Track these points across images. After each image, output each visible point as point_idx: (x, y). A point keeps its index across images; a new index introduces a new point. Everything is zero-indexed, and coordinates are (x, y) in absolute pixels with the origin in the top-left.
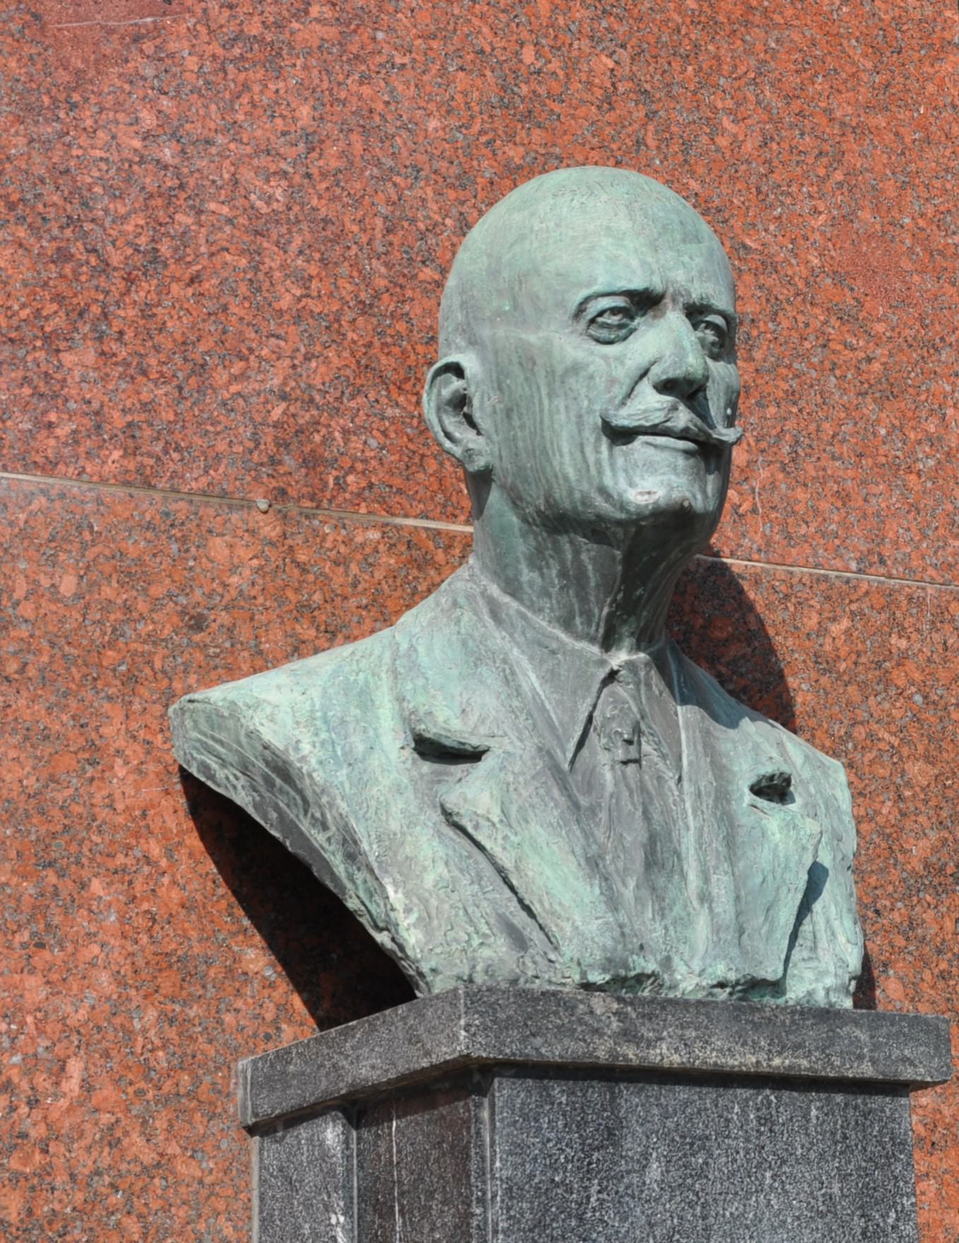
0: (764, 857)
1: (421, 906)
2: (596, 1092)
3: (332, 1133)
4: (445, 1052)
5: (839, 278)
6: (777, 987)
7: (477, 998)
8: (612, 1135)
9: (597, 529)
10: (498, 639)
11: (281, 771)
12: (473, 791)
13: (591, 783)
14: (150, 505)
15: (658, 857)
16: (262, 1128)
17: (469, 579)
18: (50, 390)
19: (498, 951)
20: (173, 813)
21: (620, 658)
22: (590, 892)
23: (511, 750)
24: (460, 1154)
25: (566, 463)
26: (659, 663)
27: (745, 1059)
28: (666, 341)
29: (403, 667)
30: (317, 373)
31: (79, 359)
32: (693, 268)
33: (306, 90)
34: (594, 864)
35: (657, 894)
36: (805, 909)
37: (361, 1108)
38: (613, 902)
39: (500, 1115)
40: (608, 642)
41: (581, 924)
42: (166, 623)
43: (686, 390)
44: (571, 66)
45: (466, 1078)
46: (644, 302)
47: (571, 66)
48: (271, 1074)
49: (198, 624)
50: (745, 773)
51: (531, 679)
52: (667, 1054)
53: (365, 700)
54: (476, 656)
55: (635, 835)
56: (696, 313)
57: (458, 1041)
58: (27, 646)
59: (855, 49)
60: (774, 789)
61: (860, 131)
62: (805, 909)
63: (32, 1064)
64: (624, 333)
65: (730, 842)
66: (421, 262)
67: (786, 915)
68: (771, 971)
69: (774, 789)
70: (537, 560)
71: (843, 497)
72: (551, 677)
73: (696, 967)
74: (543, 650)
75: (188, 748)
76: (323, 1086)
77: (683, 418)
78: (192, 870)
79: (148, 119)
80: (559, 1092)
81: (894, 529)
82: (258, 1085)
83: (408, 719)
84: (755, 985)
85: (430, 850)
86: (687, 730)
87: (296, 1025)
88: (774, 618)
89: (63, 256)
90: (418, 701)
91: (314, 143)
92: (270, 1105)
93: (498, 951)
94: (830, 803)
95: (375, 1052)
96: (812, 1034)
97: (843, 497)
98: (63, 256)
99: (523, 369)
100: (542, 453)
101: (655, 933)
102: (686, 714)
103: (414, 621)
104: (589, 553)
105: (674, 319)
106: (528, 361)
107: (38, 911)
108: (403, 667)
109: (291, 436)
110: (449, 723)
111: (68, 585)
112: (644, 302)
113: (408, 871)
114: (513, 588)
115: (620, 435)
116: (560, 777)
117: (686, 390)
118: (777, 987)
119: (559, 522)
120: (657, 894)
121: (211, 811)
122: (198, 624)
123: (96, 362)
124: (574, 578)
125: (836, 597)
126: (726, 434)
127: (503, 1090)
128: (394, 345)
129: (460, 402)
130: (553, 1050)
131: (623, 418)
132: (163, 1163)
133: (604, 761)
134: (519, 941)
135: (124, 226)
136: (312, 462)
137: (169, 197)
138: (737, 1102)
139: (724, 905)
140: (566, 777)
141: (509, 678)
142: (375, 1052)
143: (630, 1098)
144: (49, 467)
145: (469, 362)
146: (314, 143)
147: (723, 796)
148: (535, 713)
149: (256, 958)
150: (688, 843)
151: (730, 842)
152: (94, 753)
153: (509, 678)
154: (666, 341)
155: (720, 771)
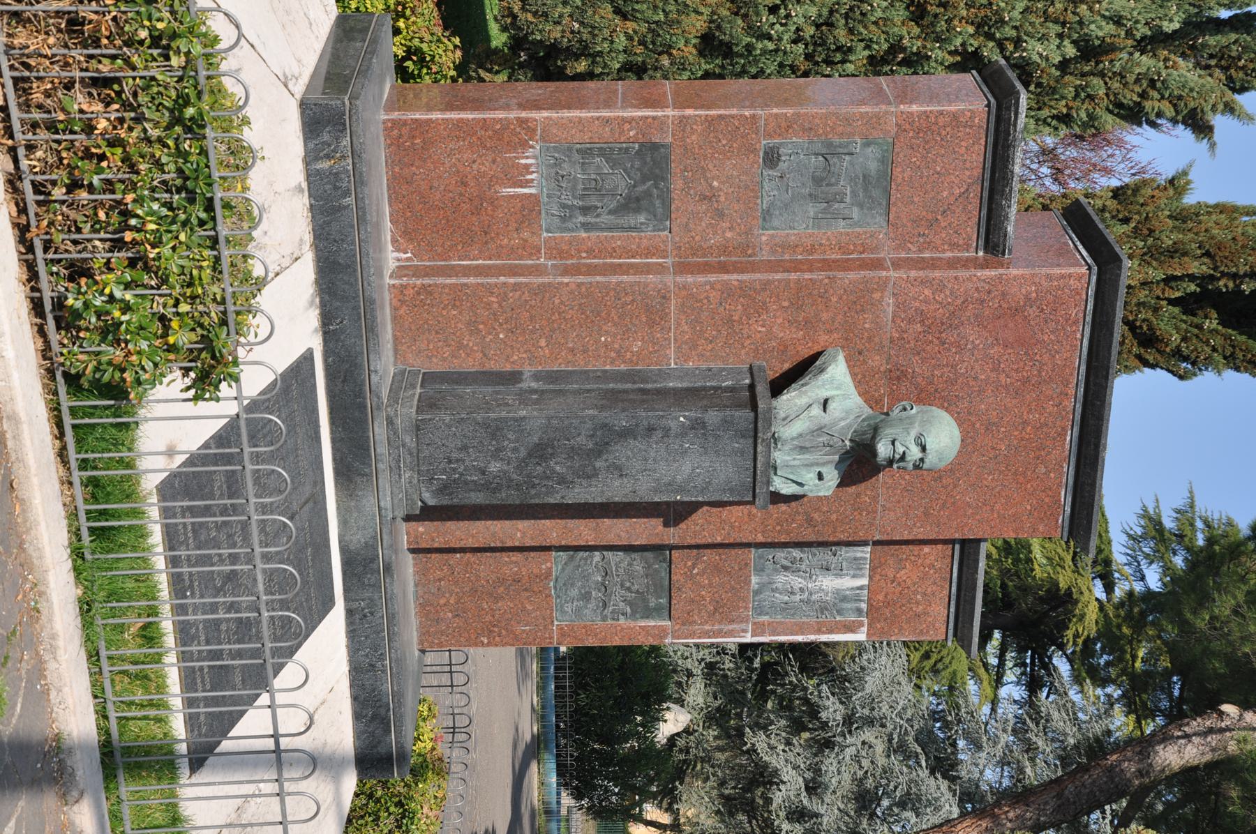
0: (804, 473)
1: (791, 399)
2: (752, 433)
3: (747, 381)
4: (759, 403)
5: (953, 503)
6: (775, 474)
7: (770, 410)
8: (743, 437)
9: (874, 438)
10: (852, 417)
11: (822, 370)
12: (816, 411)
13: (819, 435)
14: (886, 343)
15: (803, 449)
16: (751, 368)
17: (868, 411)
18: (911, 321)
19: (782, 415)
20: (817, 349)
21: (848, 443)
22: (795, 434)
23: (826, 419)
24: (739, 406)
25: (888, 431)
26: (847, 452)
27: (759, 465)
28: (914, 453)
29: (846, 397)
30: (919, 380)
31: (919, 327)
32: (931, 460)
33: (988, 378)
34: (800, 435)
35: (795, 449)
36: (794, 482)
37: (752, 387)
38: (792, 439)
39: (747, 414)
40: (851, 440)
41: (788, 432)
42: (860, 346)
43: (903, 458)
44: (1001, 439)
45: (754, 407)
46: (924, 449)
47: (1001, 439)
48: (761, 369)
49: (860, 353)
50: (824, 470)
51: (842, 424)
52: (760, 448)
53: (838, 388)
54: (848, 412)
55: (807, 444)
56: (922, 460)
57: (761, 405)
58: (853, 317)
59: (1014, 510)
60: (820, 476)
61: (992, 510)
62: (794, 482)
63: (764, 321)
64: (917, 444)
65: (807, 465)
66: (947, 404)
67: (791, 477)
68: (779, 472)
69: (820, 476)
70: (869, 425)
71: (899, 502)
72: (843, 428)
73: (779, 456)
74: (849, 426)
75: (830, 351)
76: (757, 379)
77: (897, 456)
78: (806, 353)
79: (977, 342)
80: (752, 426)
81: (892, 513)
82: (759, 367)
83: (833, 397)
84: (775, 469)
85: (804, 401)
86: (450, 258)
87: (772, 375)
88: (868, 484)
89: (942, 324)
90: (837, 399)
91: (975, 379)
92: (755, 369)
93: (782, 415)
94: (819, 490)
95: (762, 390)
96: (764, 479)
97: (899, 502)
98: (942, 324)
99: (910, 421)
100: (891, 426)
101: (786, 448)
102: (837, 458)
103: (859, 400)
104: (869, 436)
105: (920, 455)
106: (911, 424)
107: (796, 321)
108: (846, 397)
109: (904, 373)
110: (832, 406)
111: (867, 326)
112: (924, 449)
113: (799, 396)
114: (864, 420)
115: (893, 443)
116: (820, 429)
117: (903, 458)
118: (775, 474)
119: (876, 430)
120: (795, 449)
121: (818, 355)
122: (860, 353)
123: (246, 398)
124: (864, 433)
125: (875, 499)
126: (895, 466)
127: (752, 414)
128: (925, 396)
129: (905, 409)
130: (760, 425)
131: (897, 443)
132: (744, 347)
133: (824, 439)
134: (784, 419)
135: (951, 337)
136: (898, 378)
137: (959, 346)
138: (750, 463)
139: (792, 463)
140: (820, 430)
141: (842, 419)
142: (762, 390)
143: (751, 440)
144: (893, 321)
145: (914, 411)
146: (975, 379)
147: (817, 464)
148: (835, 424)
149: (787, 366)
150: (807, 456)
151: (807, 465)
152: (830, 332)
153: (842, 419)
154: (914, 453)
155: (824, 464)
